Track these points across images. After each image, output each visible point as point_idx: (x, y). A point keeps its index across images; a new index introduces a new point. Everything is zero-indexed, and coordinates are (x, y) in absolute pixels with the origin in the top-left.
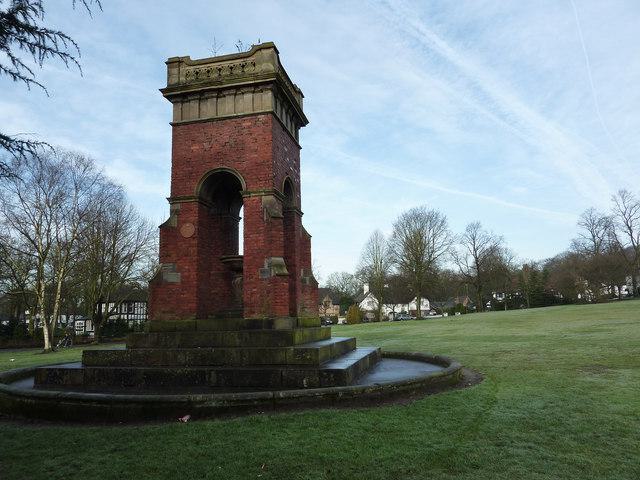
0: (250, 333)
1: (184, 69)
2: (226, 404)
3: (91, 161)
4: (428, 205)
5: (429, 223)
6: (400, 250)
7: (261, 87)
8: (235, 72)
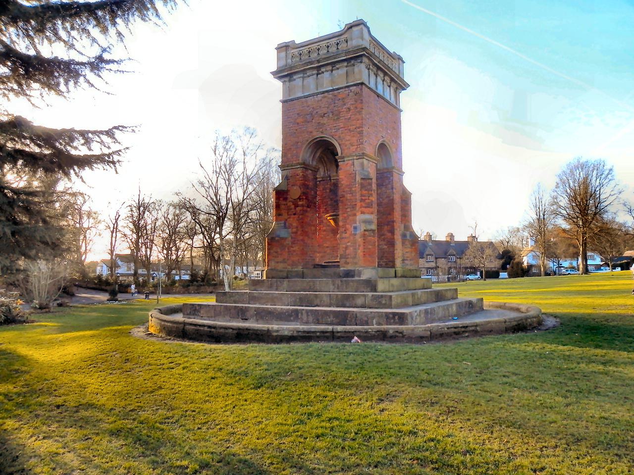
0: (341, 281)
1: (292, 51)
2: (295, 334)
3: (255, 130)
4: (591, 156)
5: (595, 172)
6: (564, 201)
7: (352, 62)
8: (321, 53)
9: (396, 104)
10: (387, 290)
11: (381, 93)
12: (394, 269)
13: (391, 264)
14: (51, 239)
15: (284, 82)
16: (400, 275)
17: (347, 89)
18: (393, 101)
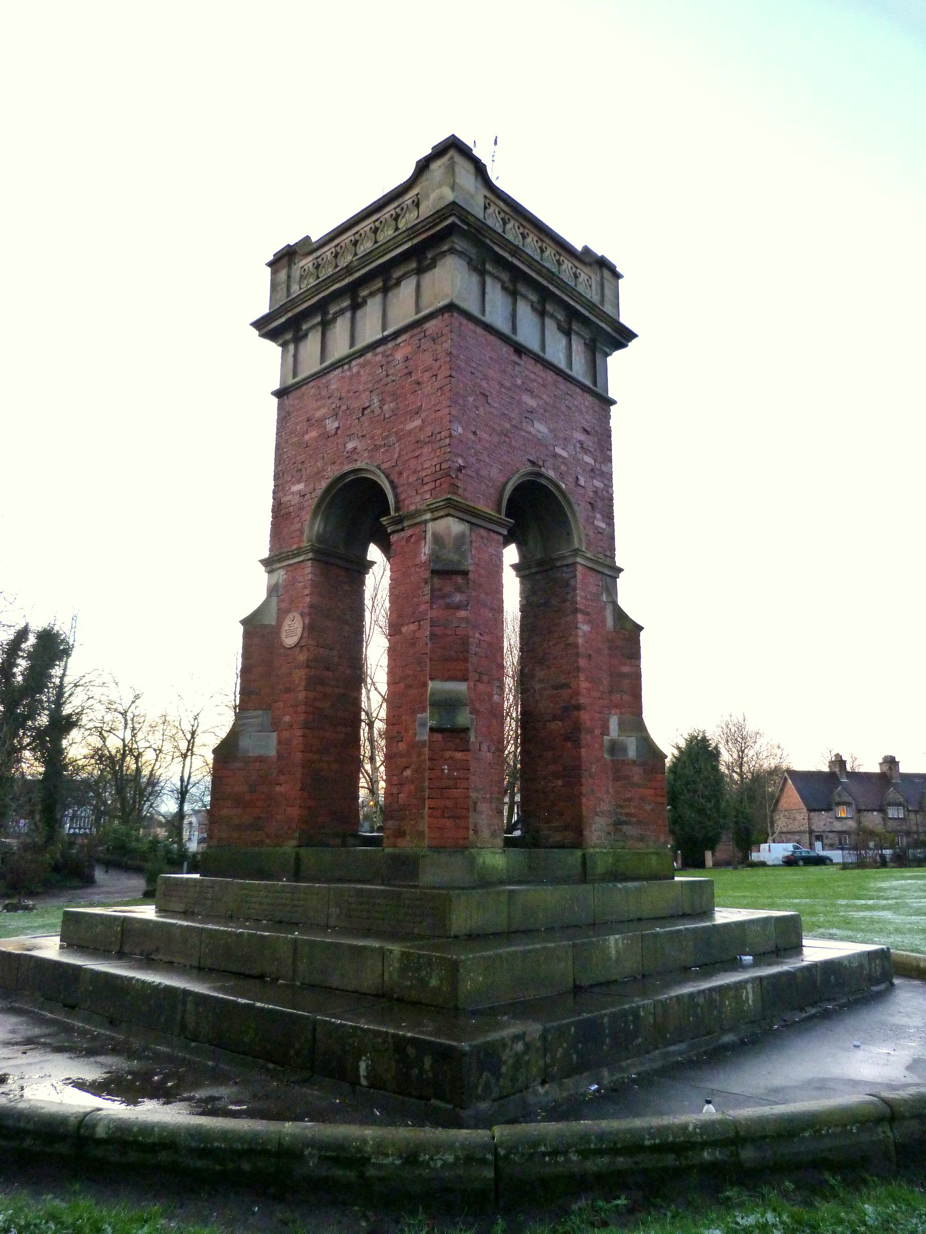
9: (595, 384)
10: (222, 968)
11: (534, 345)
12: (579, 853)
13: (570, 836)
14: (189, 777)
15: (284, 345)
16: (600, 869)
17: (415, 331)
18: (579, 370)
